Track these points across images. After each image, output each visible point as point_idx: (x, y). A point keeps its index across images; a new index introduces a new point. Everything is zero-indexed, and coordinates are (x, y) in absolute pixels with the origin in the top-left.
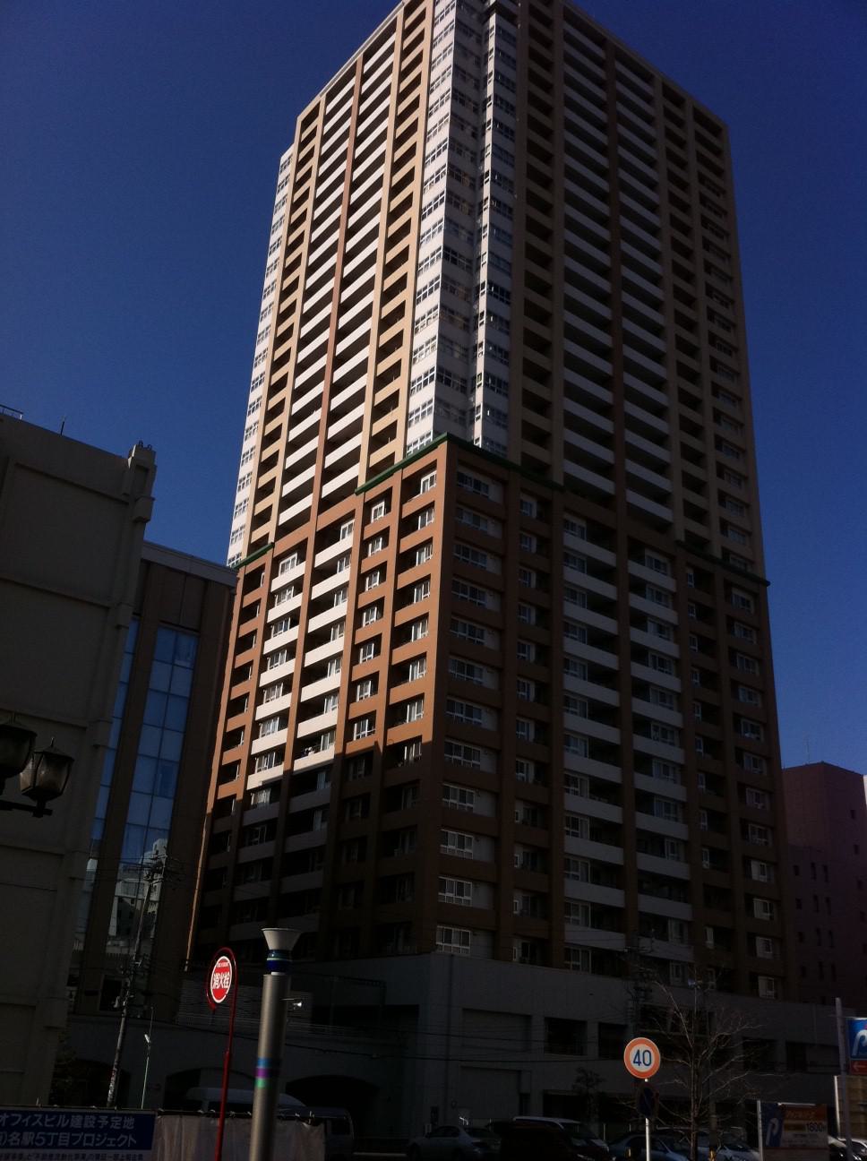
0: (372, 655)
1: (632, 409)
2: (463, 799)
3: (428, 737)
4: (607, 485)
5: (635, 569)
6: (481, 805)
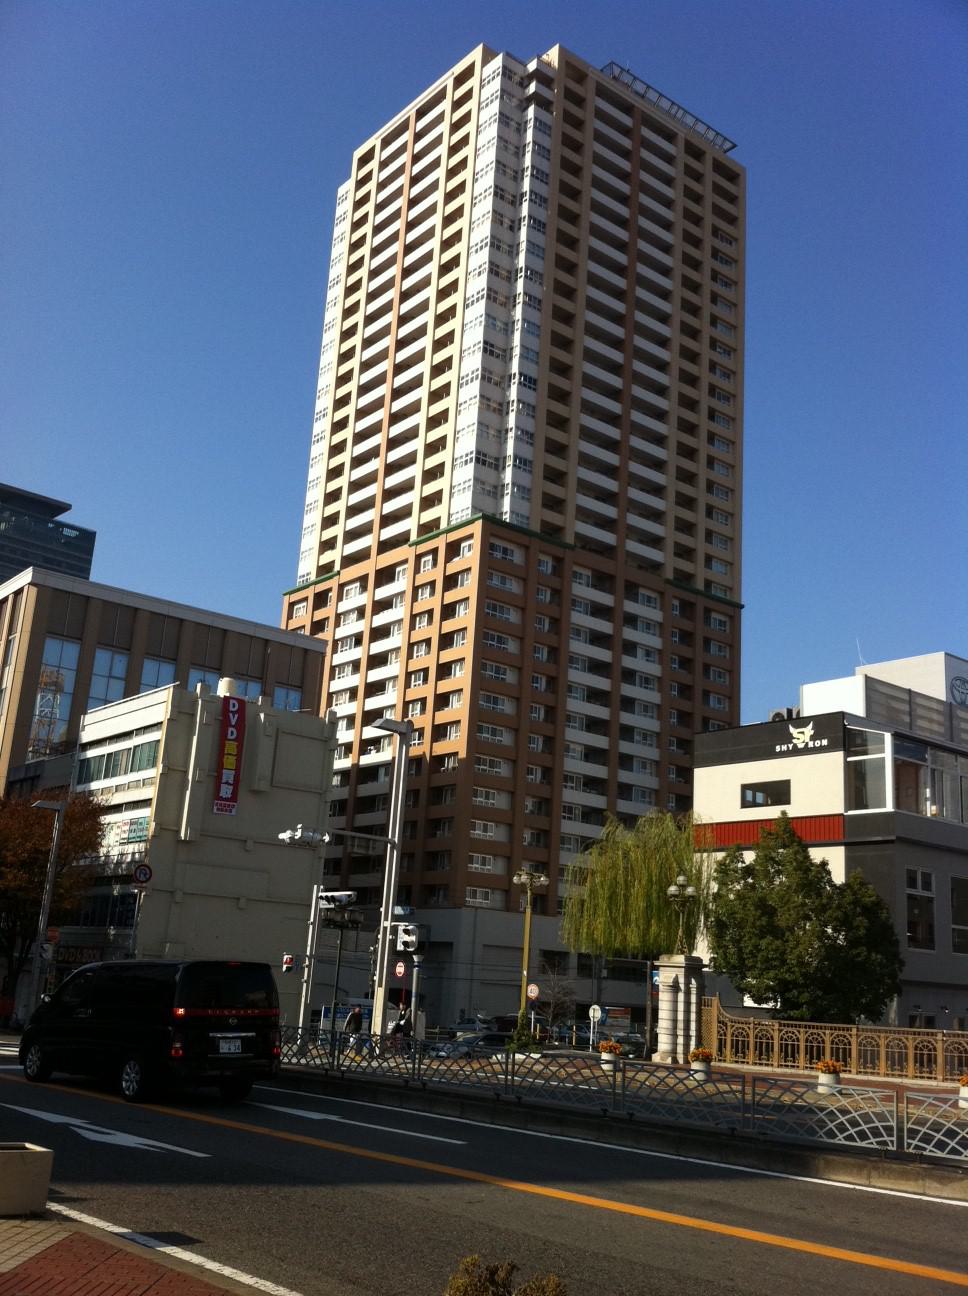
0: (421, 682)
1: (644, 223)
2: (487, 798)
3: (463, 754)
4: (608, 538)
5: (630, 607)
6: (500, 801)
